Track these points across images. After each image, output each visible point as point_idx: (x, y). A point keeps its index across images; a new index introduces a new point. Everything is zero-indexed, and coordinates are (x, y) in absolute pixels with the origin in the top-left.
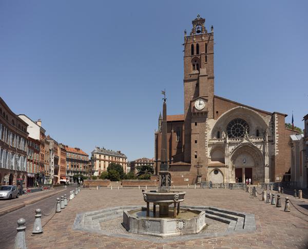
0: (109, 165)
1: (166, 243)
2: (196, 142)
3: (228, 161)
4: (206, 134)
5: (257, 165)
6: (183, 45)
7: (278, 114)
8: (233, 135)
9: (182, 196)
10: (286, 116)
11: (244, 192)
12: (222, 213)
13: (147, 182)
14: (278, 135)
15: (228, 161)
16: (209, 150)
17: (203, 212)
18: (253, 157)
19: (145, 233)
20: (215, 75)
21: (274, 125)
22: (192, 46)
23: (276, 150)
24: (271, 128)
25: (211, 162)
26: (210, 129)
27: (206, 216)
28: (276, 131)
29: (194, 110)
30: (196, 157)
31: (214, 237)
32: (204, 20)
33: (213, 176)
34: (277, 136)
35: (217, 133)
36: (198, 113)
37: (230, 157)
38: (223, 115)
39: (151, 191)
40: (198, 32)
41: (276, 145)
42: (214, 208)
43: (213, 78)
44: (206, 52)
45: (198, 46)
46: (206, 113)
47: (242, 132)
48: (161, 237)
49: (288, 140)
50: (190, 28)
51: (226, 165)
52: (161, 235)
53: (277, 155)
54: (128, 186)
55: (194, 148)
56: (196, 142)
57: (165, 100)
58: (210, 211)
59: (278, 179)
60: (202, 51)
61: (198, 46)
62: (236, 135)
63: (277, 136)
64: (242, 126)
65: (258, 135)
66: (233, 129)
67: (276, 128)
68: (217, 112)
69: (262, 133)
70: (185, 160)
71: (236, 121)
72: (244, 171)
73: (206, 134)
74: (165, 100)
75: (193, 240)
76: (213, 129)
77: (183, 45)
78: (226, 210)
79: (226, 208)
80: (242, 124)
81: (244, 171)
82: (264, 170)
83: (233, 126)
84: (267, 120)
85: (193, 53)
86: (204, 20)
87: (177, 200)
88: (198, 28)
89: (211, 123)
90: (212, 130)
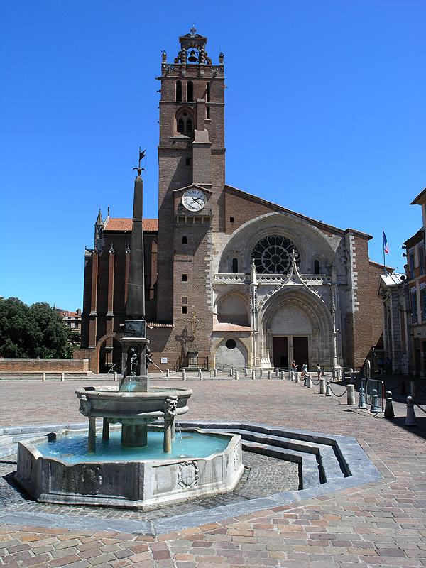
1: (174, 535)
2: (185, 278)
3: (256, 323)
4: (209, 262)
5: (318, 330)
6: (159, 79)
7: (357, 234)
9: (183, 400)
10: (370, 238)
11: (289, 383)
12: (276, 438)
13: (63, 364)
14: (356, 273)
15: (256, 323)
16: (214, 296)
17: (237, 439)
18: (308, 315)
19: (88, 500)
20: (227, 145)
21: (349, 254)
22: (179, 85)
23: (354, 303)
24: (343, 259)
25: (218, 326)
26: (215, 253)
27: (245, 448)
28: (353, 266)
30: (185, 310)
31: (296, 504)
32: (205, 40)
33: (224, 353)
34: (355, 276)
35: (232, 264)
36: (190, 219)
37: (261, 314)
38: (244, 226)
39: (87, 389)
40: (192, 59)
41: (354, 294)
42: (253, 425)
43: (223, 152)
46: (208, 219)
47: (285, 263)
48: (135, 509)
49: (377, 284)
50: (174, 50)
51: (251, 329)
52: (135, 503)
54: (13, 374)
55: (180, 291)
56: (185, 278)
57: (139, 172)
58: (249, 433)
59: (359, 359)
62: (273, 269)
63: (355, 276)
64: (285, 250)
65: (317, 270)
66: (267, 256)
67: (353, 260)
68: (232, 220)
69: (326, 267)
70: (159, 317)
71: (272, 240)
72: (290, 342)
73: (209, 262)
74: (139, 172)
75: (243, 517)
76: (223, 253)
77: (159, 79)
79: (283, 425)
81: (290, 342)
82: (331, 340)
83: (266, 250)
84: (335, 243)
86: (205, 40)
87: (173, 410)
88: (193, 52)
89: (218, 242)
90: (220, 255)
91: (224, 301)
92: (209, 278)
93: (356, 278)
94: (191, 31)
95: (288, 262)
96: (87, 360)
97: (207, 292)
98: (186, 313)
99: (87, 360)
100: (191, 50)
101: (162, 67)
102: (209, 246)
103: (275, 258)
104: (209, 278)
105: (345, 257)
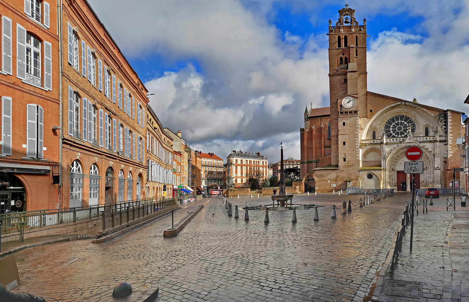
0: (247, 180)
2: (344, 143)
4: (357, 140)
7: (452, 112)
8: (394, 134)
14: (452, 135)
22: (339, 38)
24: (444, 127)
29: (341, 109)
34: (451, 136)
44: (356, 51)
45: (346, 38)
47: (405, 130)
53: (451, 158)
56: (344, 143)
60: (352, 44)
61: (346, 38)
63: (451, 136)
66: (394, 127)
73: (357, 134)
78: (8, 10)
80: (405, 121)
85: (339, 46)
91: (367, 154)
92: (358, 143)
93: (452, 138)
94: (345, 6)
95: (398, 135)
96: (298, 187)
97: (356, 150)
98: (345, 161)
99: (298, 187)
100: (345, 17)
101: (329, 28)
103: (399, 130)
104: (358, 143)
105: (445, 125)
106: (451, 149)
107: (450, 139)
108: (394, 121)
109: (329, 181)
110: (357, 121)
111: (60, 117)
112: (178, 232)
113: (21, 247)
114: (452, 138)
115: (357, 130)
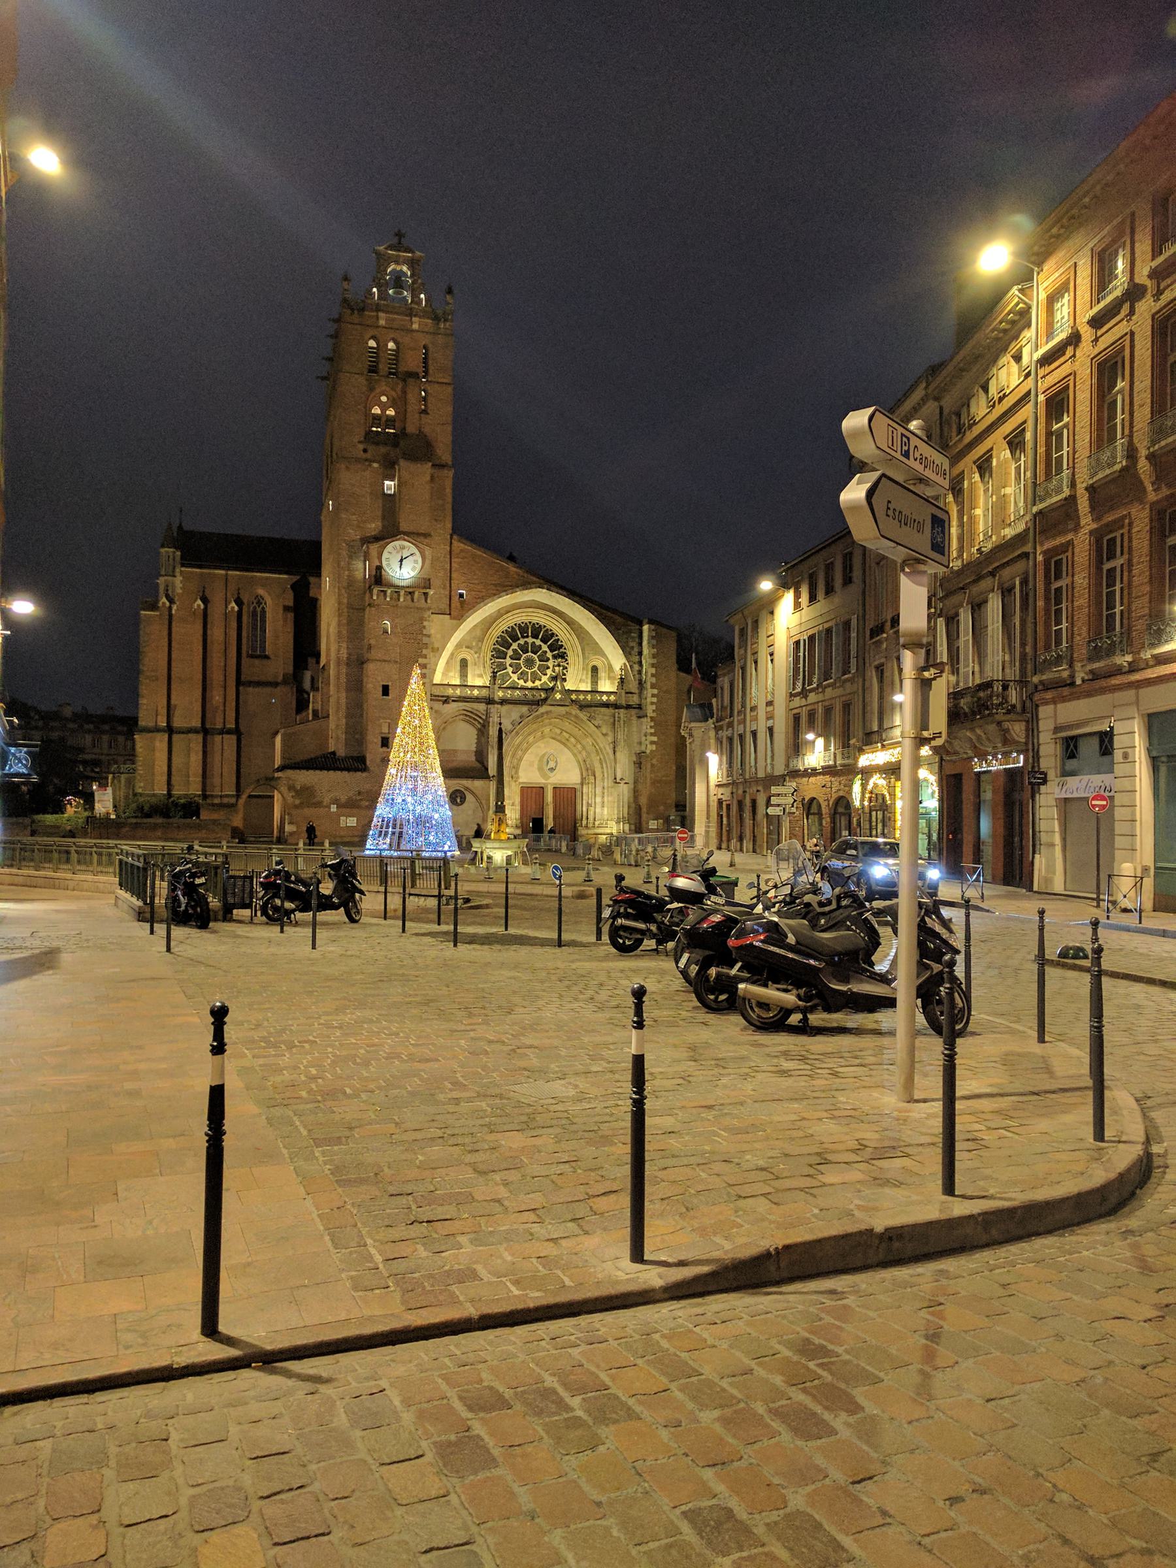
14: (655, 691)
34: (653, 696)
63: (653, 696)
83: (515, 646)
93: (655, 700)
102: (425, 640)
106: (653, 731)
107: (652, 703)
108: (515, 639)
109: (334, 808)
110: (425, 623)
111: (846, 1179)
112: (314, 804)
113: (33, 872)
114: (655, 700)
115: (425, 651)
